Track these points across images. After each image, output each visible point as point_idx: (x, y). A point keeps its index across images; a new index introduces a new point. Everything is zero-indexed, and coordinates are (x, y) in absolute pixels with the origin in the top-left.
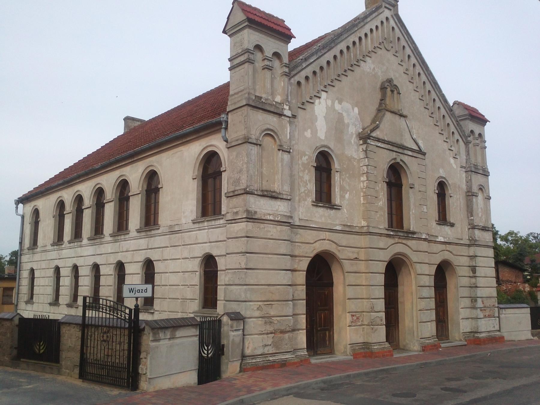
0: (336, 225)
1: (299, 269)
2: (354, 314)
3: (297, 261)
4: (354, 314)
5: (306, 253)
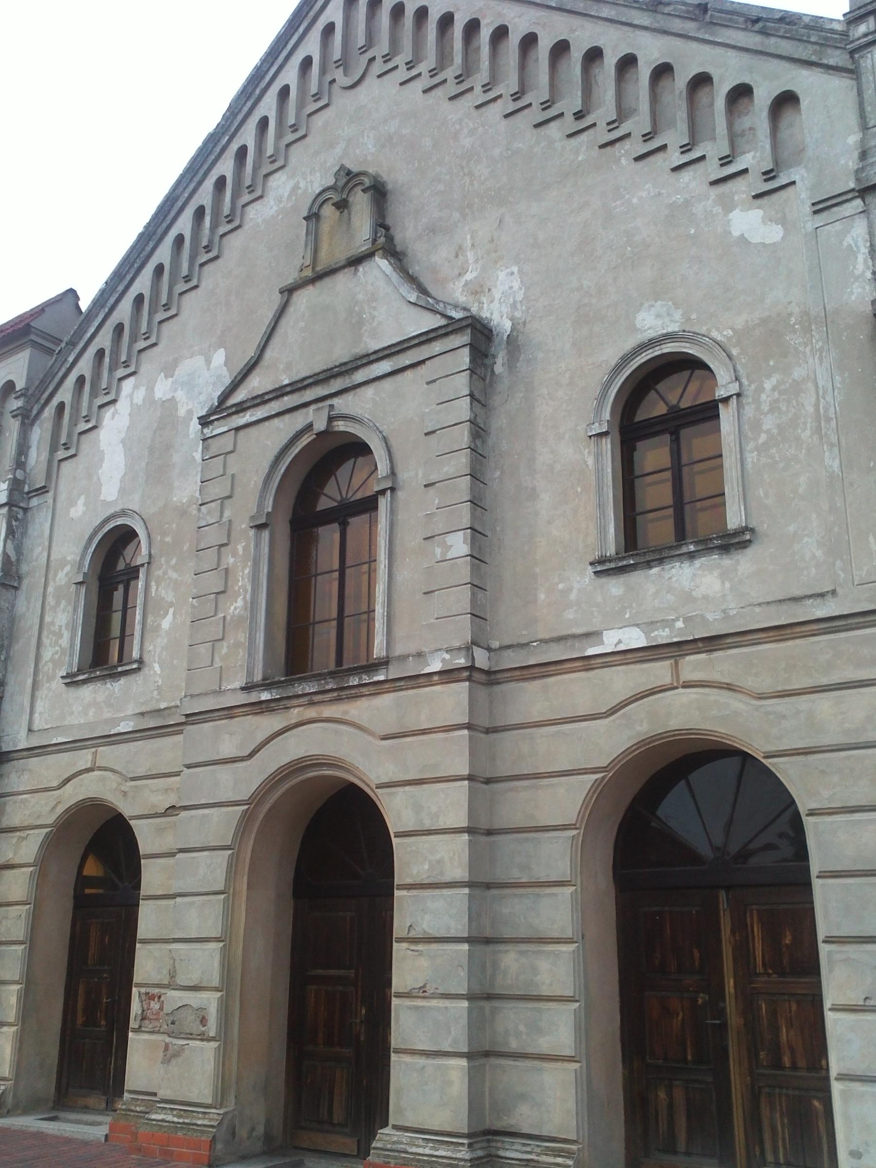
0: (116, 721)
1: (17, 861)
2: (156, 991)
3: (14, 840)
4: (156, 991)
5: (39, 817)
